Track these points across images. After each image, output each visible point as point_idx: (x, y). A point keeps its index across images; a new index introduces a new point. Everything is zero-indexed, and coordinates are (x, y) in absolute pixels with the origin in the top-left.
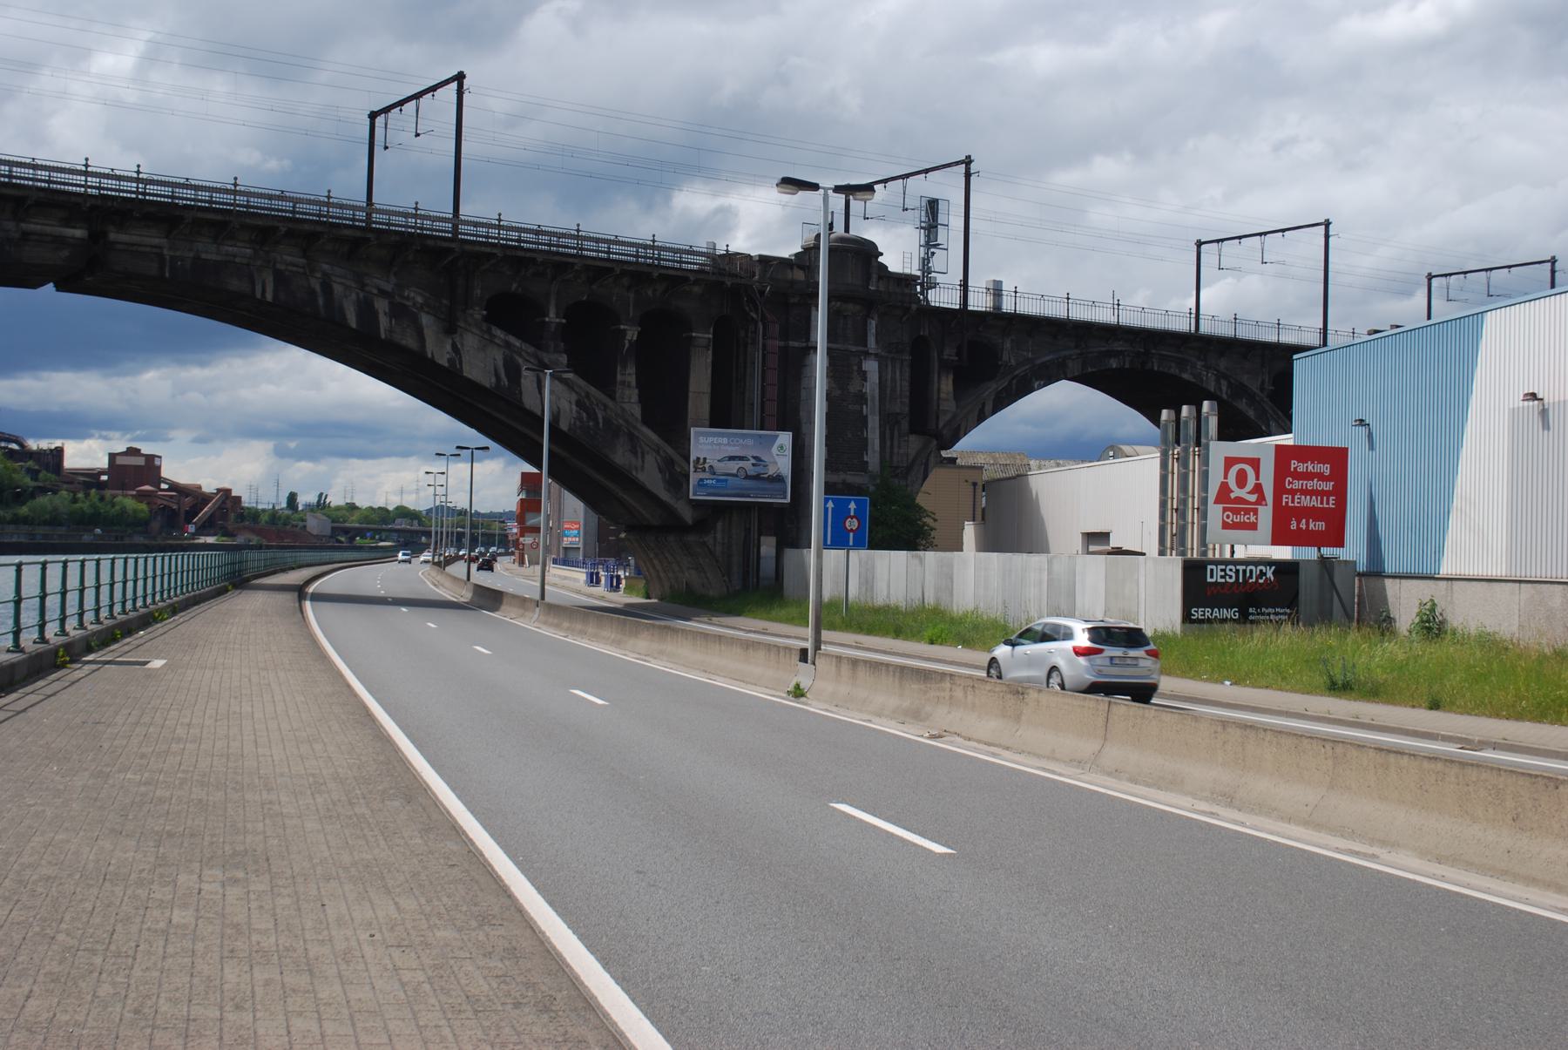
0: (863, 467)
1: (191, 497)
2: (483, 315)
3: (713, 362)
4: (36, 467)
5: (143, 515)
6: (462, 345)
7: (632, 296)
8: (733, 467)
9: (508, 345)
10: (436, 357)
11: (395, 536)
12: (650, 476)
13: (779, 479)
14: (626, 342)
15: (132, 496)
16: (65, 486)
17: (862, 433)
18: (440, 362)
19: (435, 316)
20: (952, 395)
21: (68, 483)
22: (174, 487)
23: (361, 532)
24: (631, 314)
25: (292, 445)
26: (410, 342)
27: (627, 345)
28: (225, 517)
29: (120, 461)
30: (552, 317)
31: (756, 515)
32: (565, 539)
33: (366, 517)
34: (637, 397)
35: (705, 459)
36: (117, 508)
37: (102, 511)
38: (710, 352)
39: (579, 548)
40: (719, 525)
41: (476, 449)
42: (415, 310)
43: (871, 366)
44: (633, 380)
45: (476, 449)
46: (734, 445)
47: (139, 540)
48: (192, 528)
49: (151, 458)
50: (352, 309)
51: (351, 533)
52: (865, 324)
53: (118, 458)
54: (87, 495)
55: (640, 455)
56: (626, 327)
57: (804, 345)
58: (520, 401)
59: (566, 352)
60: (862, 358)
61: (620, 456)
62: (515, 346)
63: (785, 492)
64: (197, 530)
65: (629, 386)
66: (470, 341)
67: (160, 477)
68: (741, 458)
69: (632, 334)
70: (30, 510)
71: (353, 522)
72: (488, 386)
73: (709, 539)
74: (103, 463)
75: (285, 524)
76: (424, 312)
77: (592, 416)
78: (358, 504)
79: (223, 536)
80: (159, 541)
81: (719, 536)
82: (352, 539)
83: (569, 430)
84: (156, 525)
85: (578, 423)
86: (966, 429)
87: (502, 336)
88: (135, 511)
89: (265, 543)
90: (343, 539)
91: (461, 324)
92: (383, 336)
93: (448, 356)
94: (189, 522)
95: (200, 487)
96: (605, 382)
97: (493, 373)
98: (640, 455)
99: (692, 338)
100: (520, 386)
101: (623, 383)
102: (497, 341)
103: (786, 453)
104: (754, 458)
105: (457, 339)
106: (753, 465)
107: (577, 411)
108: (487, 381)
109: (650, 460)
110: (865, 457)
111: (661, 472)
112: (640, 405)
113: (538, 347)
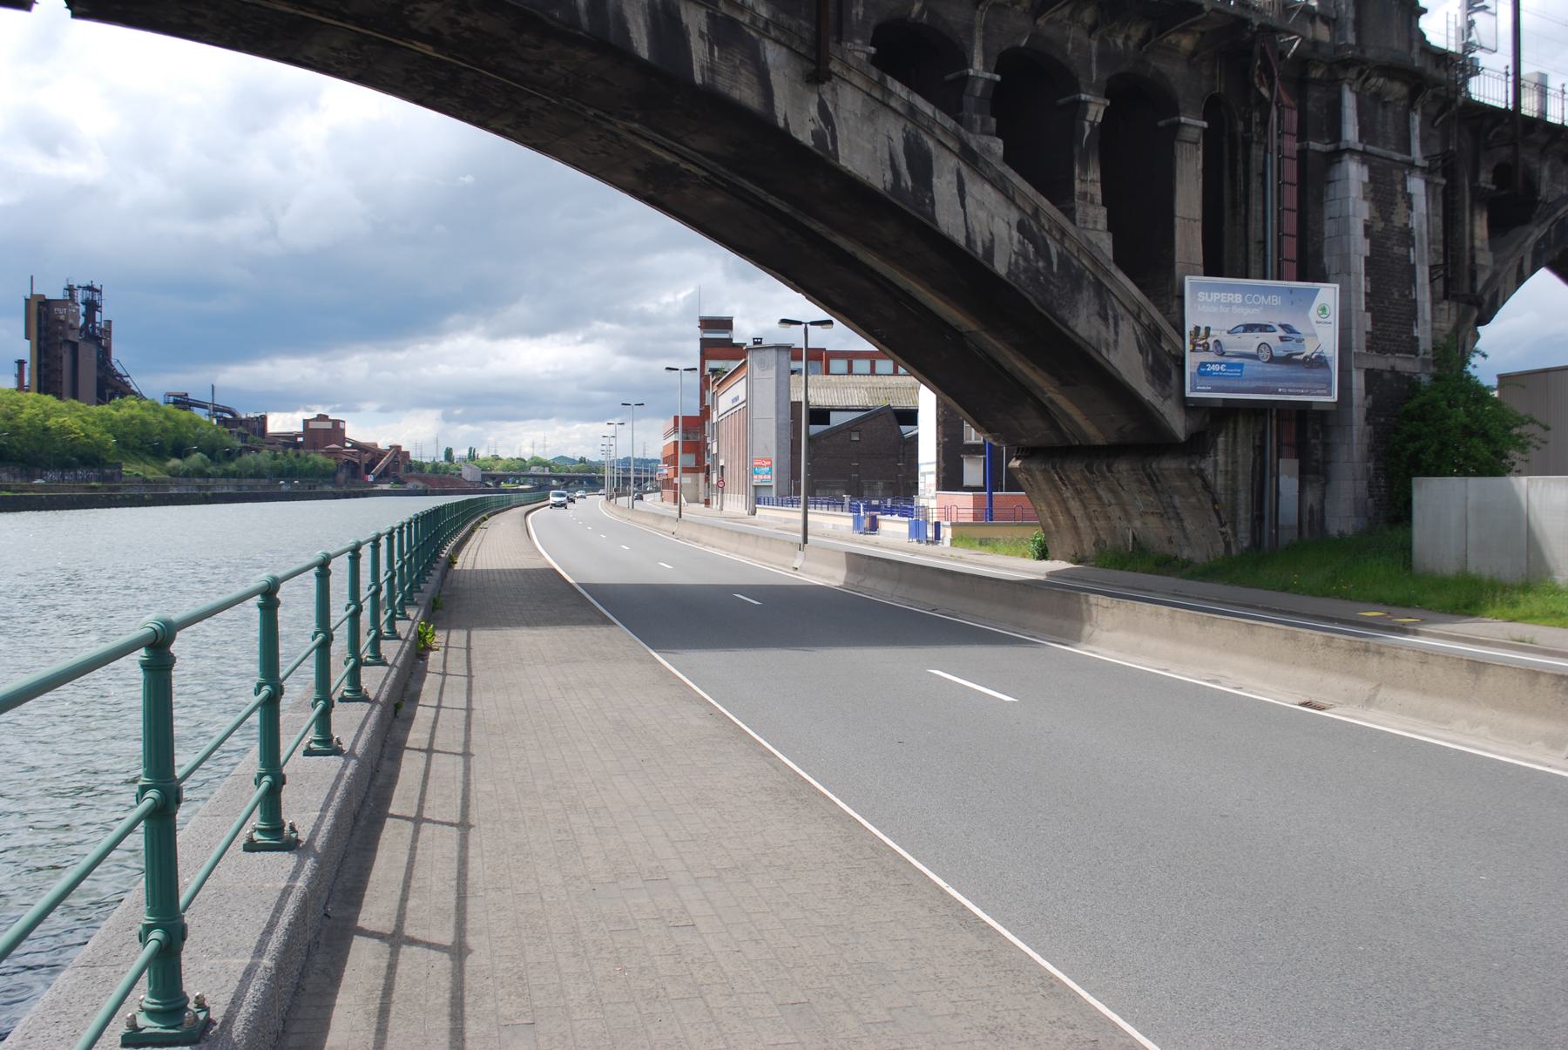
0: (1412, 347)
1: (369, 454)
2: (868, 54)
3: (1203, 170)
4: (245, 432)
5: (331, 468)
6: (836, 106)
7: (1095, 44)
8: (1251, 342)
9: (912, 112)
10: (791, 128)
11: (531, 480)
12: (1128, 362)
13: (1319, 362)
14: (1087, 124)
15: (323, 453)
16: (267, 446)
17: (1411, 293)
18: (800, 137)
19: (789, 48)
20: (1486, 242)
21: (270, 444)
22: (356, 445)
23: (505, 478)
24: (1094, 78)
25: (458, 412)
26: (745, 94)
27: (1087, 131)
28: (397, 468)
29: (312, 425)
30: (978, 69)
31: (1274, 422)
32: (755, 477)
33: (508, 466)
34: (1105, 221)
35: (1208, 329)
36: (311, 463)
37: (297, 465)
38: (1200, 153)
39: (771, 486)
40: (1221, 440)
41: (812, 323)
42: (753, 34)
43: (1416, 185)
44: (1096, 191)
45: (812, 323)
46: (1252, 306)
47: (328, 488)
48: (370, 478)
49: (336, 423)
50: (641, 21)
51: (498, 479)
52: (1407, 122)
53: (310, 423)
54: (285, 453)
55: (1111, 321)
56: (1088, 97)
57: (1330, 147)
58: (933, 219)
59: (999, 134)
60: (1407, 172)
61: (1084, 323)
62: (923, 114)
63: (1330, 384)
64: (375, 479)
65: (1092, 202)
66: (849, 102)
67: (345, 438)
68: (1264, 328)
69: (1096, 111)
70: (237, 466)
71: (498, 470)
72: (880, 186)
73: (1207, 465)
74: (300, 429)
75: (445, 473)
76: (770, 38)
77: (1042, 251)
78: (500, 456)
79: (395, 483)
80: (345, 489)
81: (1221, 458)
82: (498, 484)
83: (1010, 272)
84: (342, 476)
85: (1021, 261)
86: (1504, 297)
87: (904, 94)
88: (325, 465)
89: (430, 488)
90: (491, 484)
91: (835, 67)
92: (698, 79)
93: (812, 127)
94: (368, 473)
95: (376, 445)
96: (1059, 191)
97: (888, 163)
98: (1111, 321)
99: (1179, 125)
100: (932, 192)
101: (1084, 195)
102: (893, 103)
103: (1330, 319)
104: (1283, 327)
105: (827, 97)
106: (1282, 339)
107: (1019, 242)
108: (878, 178)
109: (1127, 329)
110: (1415, 331)
111: (1141, 351)
112: (1111, 235)
113: (959, 120)
